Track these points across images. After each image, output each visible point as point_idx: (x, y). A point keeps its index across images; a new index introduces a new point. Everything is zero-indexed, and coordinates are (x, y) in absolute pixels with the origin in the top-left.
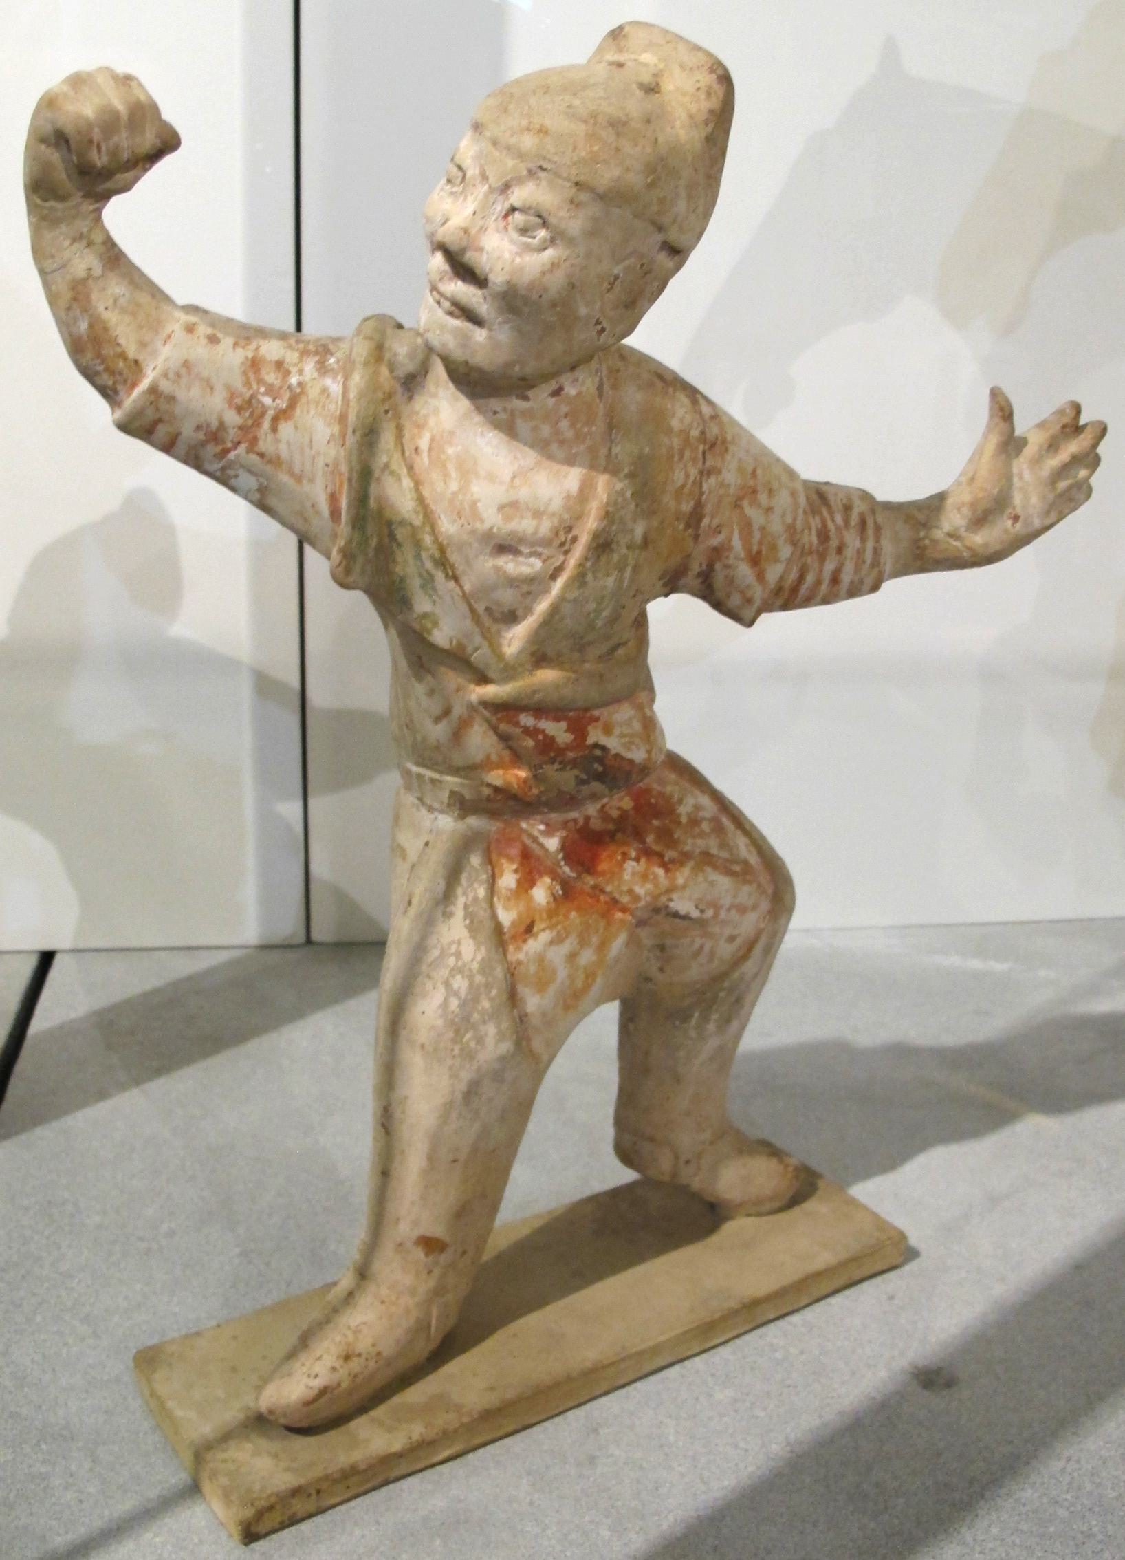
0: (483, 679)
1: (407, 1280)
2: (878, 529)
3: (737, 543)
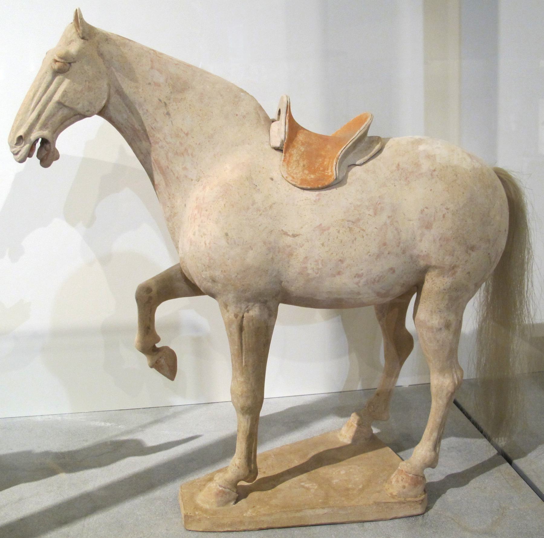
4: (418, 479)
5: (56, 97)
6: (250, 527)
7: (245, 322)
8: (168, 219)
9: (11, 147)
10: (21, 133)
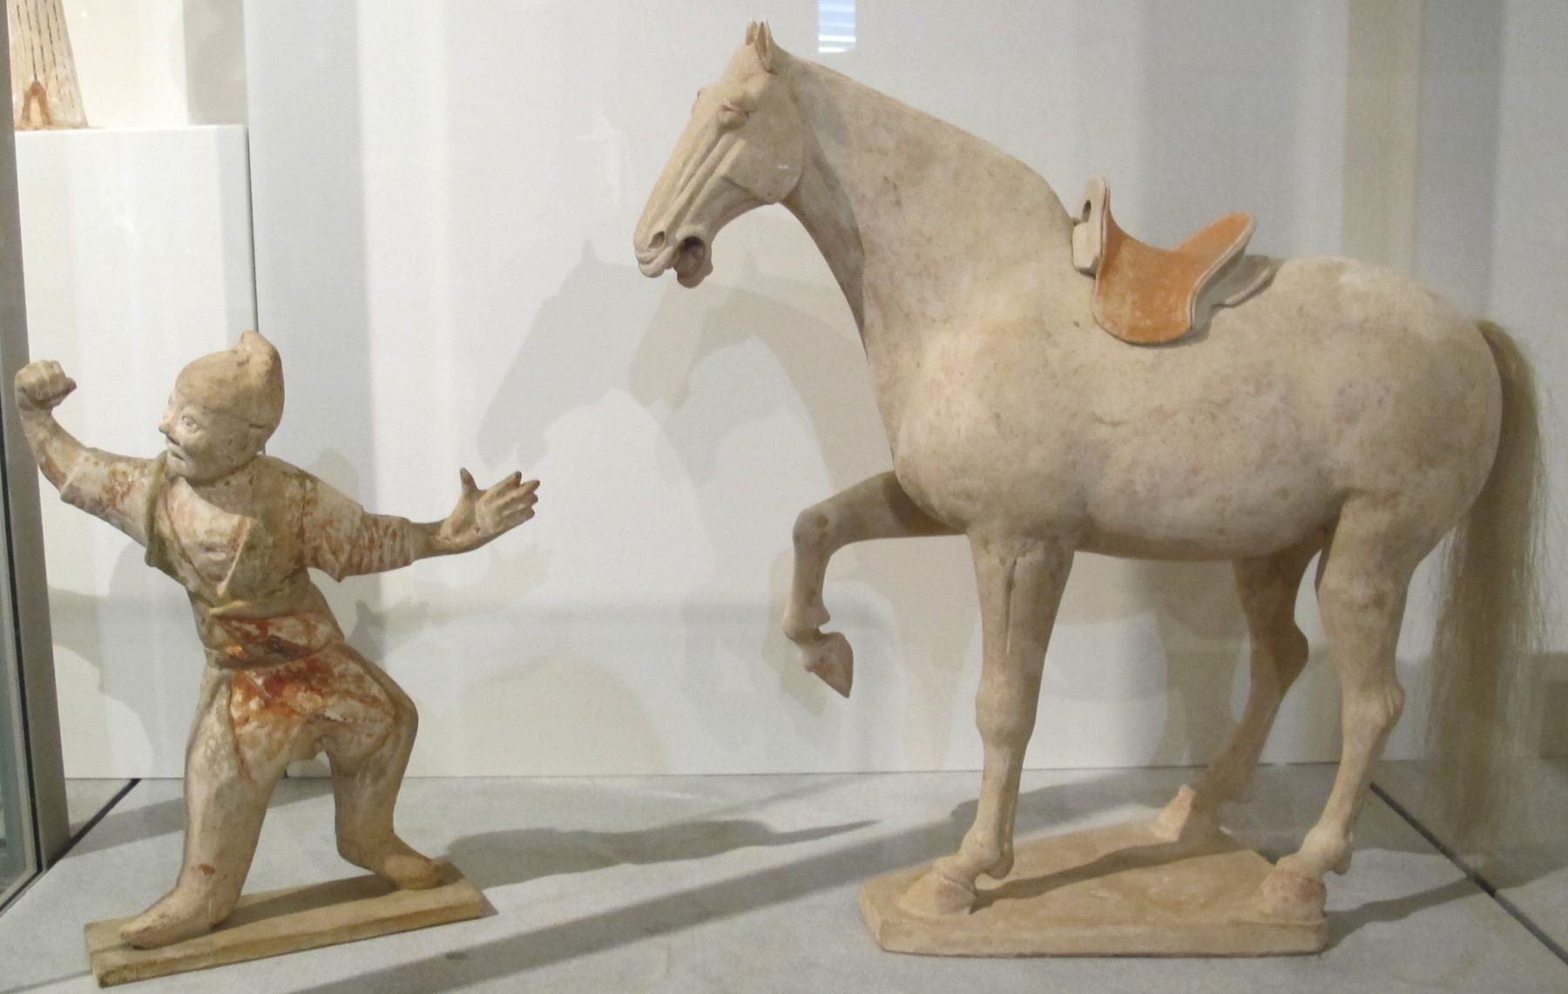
0: (213, 606)
1: (195, 885)
2: (403, 538)
3: (325, 545)
4: (1313, 889)
5: (722, 169)
6: (1001, 950)
7: (1018, 574)
8: (883, 390)
9: (638, 248)
10: (661, 226)
